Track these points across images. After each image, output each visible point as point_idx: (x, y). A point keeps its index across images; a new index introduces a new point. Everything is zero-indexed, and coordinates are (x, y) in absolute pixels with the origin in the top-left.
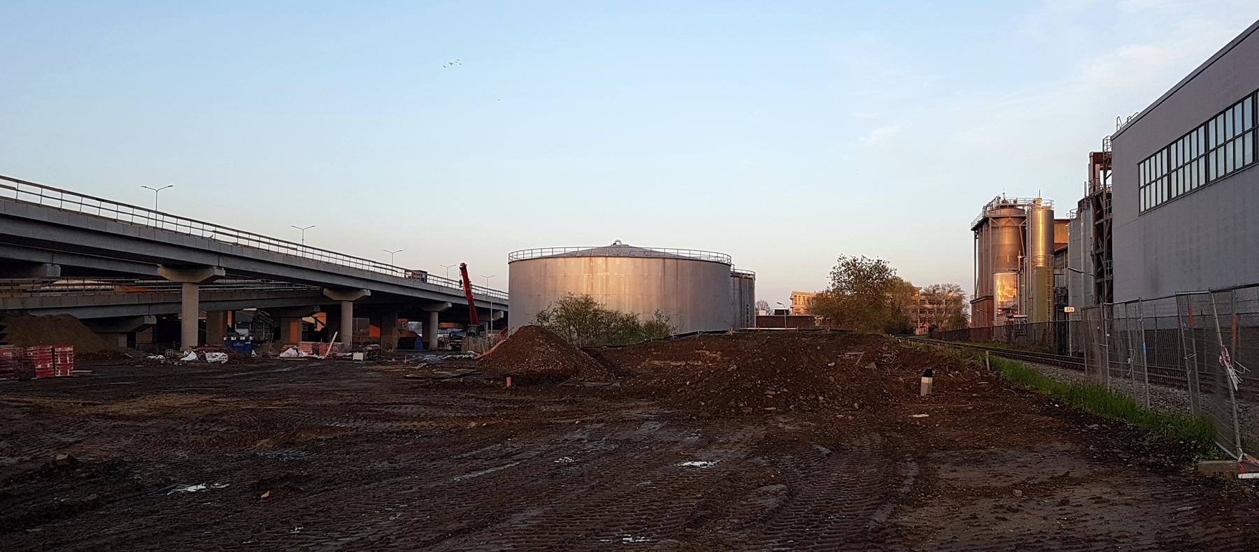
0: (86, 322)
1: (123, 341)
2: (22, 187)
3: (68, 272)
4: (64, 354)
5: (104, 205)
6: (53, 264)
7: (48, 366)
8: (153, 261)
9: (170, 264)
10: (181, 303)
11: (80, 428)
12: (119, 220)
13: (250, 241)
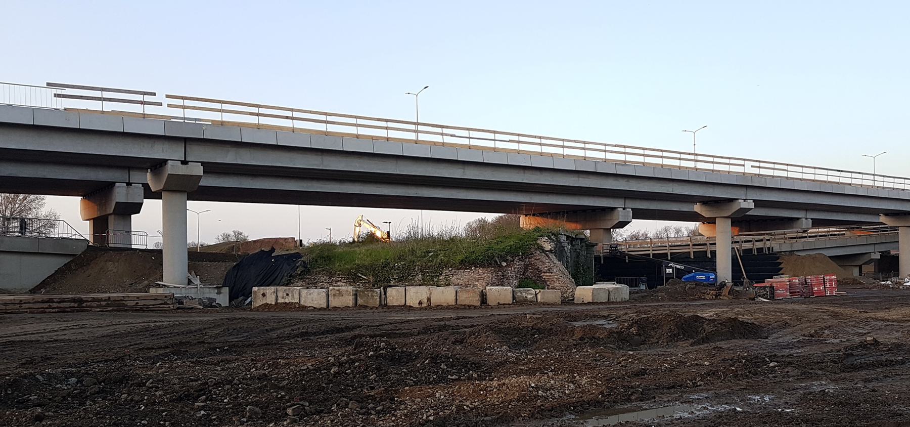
0: (833, 258)
1: (856, 271)
2: (790, 168)
3: (817, 223)
4: (831, 280)
5: (843, 174)
6: (806, 218)
7: (821, 288)
8: (876, 212)
9: (888, 213)
10: (898, 242)
11: (866, 325)
12: (853, 184)
13: (895, 179)
